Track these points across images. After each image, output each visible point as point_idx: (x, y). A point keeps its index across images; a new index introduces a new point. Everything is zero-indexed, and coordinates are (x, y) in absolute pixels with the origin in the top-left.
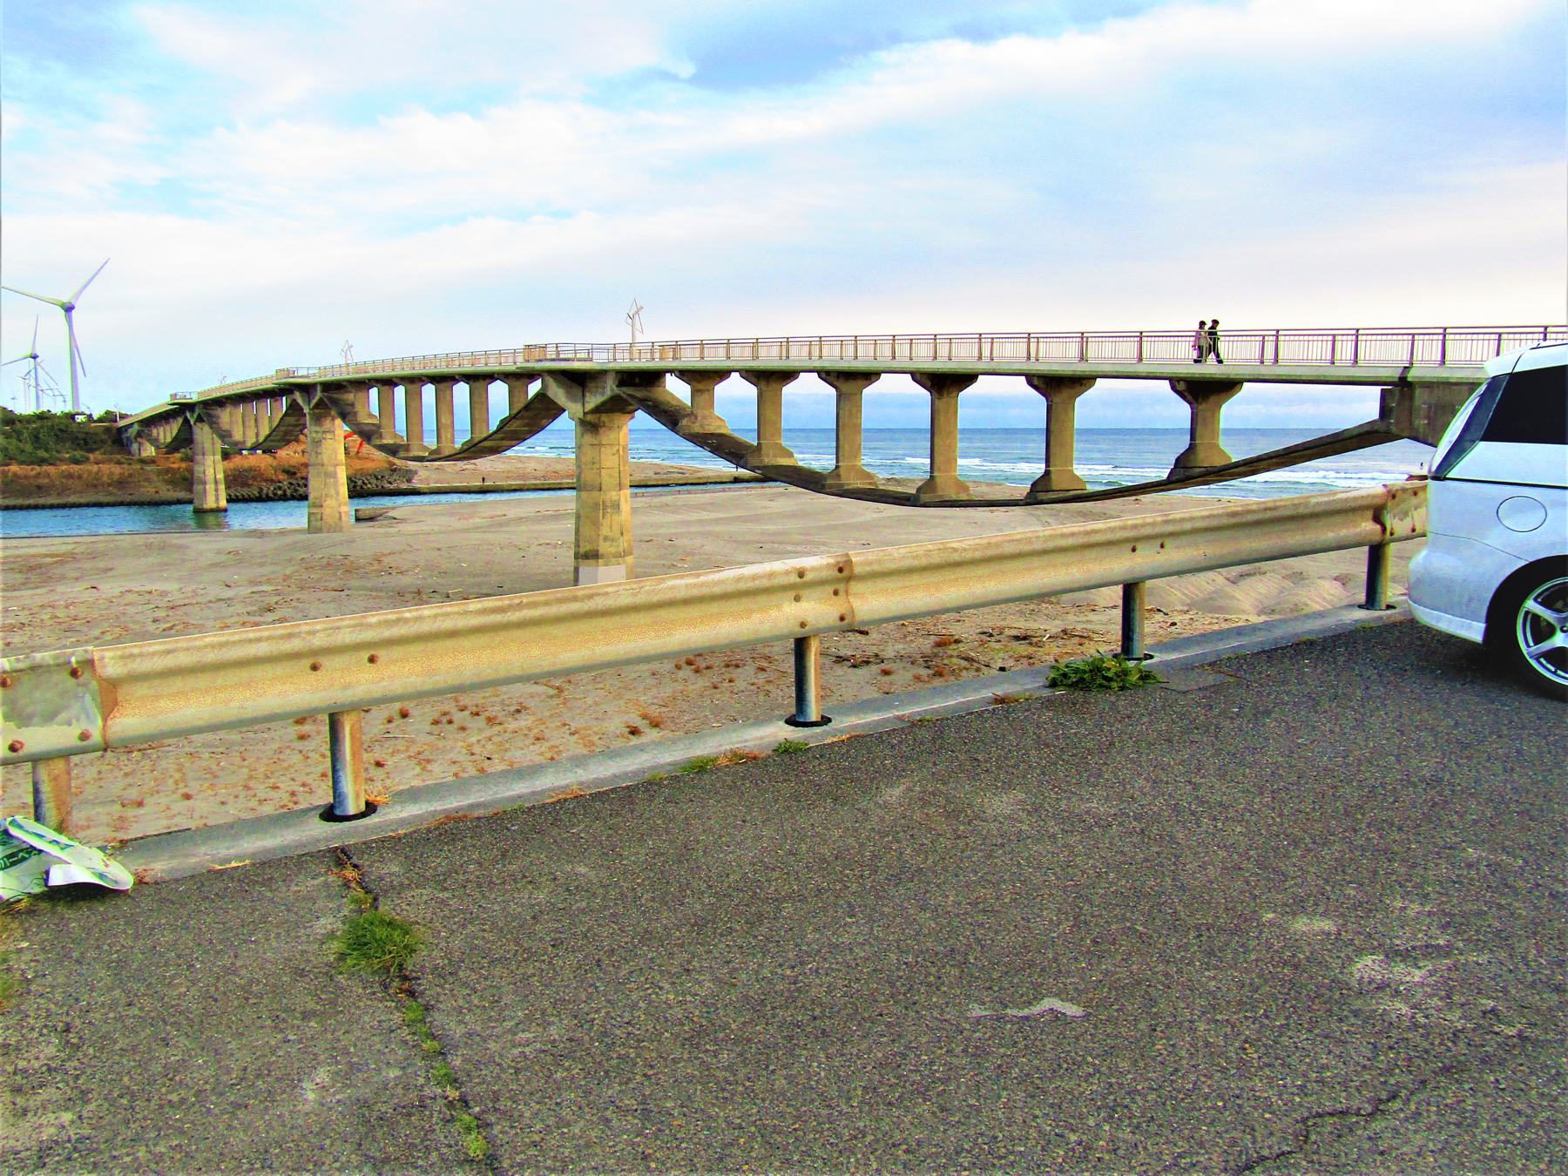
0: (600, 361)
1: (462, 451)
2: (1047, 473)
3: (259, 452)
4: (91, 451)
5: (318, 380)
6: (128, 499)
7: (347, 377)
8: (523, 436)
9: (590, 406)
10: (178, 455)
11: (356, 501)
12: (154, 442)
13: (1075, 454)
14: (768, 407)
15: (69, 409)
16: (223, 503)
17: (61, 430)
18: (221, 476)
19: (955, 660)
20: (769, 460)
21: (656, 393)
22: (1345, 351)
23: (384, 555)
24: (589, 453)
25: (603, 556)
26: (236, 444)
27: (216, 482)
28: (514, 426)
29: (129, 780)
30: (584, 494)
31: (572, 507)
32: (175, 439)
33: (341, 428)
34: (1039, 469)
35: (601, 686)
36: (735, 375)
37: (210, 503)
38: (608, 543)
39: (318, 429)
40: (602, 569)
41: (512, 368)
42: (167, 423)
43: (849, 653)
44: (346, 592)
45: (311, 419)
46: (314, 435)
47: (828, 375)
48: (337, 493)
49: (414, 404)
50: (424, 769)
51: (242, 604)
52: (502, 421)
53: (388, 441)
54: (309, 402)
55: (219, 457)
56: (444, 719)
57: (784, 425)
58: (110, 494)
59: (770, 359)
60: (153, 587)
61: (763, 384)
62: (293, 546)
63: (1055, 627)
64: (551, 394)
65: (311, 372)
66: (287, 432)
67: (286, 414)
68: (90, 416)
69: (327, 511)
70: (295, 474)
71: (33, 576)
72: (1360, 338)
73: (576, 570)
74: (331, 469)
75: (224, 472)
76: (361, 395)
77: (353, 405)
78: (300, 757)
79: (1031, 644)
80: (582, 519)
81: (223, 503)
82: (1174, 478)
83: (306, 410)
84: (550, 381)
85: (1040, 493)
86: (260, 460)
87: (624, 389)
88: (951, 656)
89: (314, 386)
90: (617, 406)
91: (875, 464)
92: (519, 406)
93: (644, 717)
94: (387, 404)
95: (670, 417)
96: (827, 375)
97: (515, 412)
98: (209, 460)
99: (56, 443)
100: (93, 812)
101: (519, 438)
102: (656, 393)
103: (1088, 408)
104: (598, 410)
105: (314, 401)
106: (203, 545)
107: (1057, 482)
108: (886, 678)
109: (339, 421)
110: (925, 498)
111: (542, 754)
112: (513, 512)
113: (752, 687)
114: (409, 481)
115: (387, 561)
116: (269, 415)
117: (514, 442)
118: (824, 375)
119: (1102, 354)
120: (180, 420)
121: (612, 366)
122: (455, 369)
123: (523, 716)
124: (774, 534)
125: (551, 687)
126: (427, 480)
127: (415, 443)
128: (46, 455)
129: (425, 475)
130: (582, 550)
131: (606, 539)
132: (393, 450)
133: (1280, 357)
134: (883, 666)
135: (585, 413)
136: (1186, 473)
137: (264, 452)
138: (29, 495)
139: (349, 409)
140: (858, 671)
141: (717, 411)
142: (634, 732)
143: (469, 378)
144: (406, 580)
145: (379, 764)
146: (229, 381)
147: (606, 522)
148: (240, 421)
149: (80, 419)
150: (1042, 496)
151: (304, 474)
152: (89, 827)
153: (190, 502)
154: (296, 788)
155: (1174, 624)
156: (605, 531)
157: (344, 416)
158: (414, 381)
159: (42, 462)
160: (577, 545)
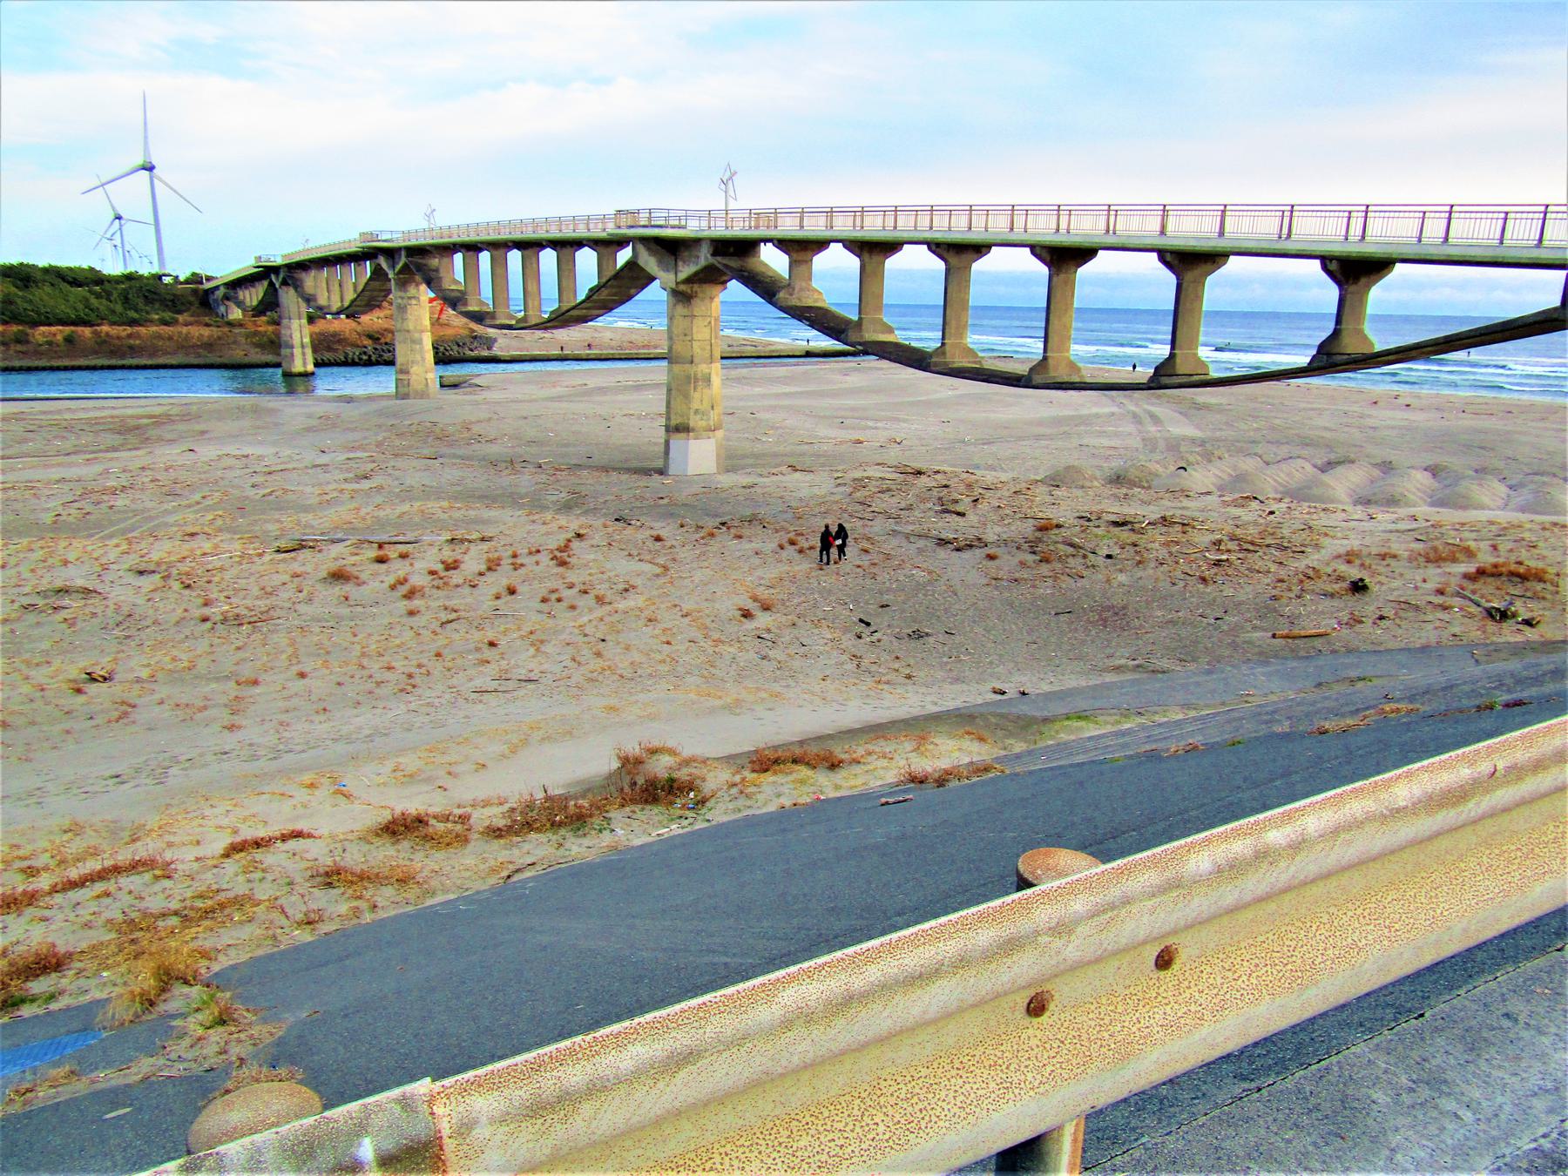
0: (693, 228)
1: (549, 321)
2: (1172, 356)
3: (343, 316)
4: (180, 312)
5: (402, 244)
6: (219, 361)
7: (431, 242)
8: (611, 305)
9: (683, 275)
10: (264, 319)
11: (441, 367)
12: (240, 304)
13: (1201, 339)
14: (869, 279)
15: (155, 270)
16: (310, 368)
17: (149, 291)
18: (307, 340)
19: (1061, 546)
20: (872, 335)
21: (751, 263)
22: (1434, 229)
23: (471, 423)
24: (681, 324)
25: (693, 430)
26: (320, 308)
27: (303, 346)
28: (604, 295)
29: (241, 655)
30: (677, 368)
31: (663, 378)
32: (261, 302)
33: (425, 293)
34: (1164, 351)
35: (706, 564)
36: (836, 248)
37: (298, 367)
38: (698, 417)
39: (402, 294)
40: (692, 442)
41: (604, 235)
42: (253, 286)
43: (951, 536)
44: (441, 460)
45: (397, 284)
46: (400, 301)
47: (938, 248)
48: (423, 359)
49: (500, 271)
50: (538, 650)
51: (337, 472)
52: (591, 290)
53: (473, 308)
54: (394, 267)
55: (304, 321)
56: (554, 596)
57: (885, 301)
58: (199, 356)
59: (874, 228)
60: (248, 450)
61: (866, 256)
62: (381, 413)
63: (1153, 513)
64: (641, 262)
65: (395, 236)
66: (370, 299)
67: (371, 279)
68: (177, 277)
69: (414, 378)
70: (378, 339)
71: (132, 440)
72: (1548, 216)
73: (667, 443)
74: (417, 335)
75: (311, 336)
76: (446, 260)
77: (437, 270)
78: (411, 633)
79: (1133, 530)
80: (673, 392)
81: (310, 368)
82: (1315, 365)
83: (391, 276)
84: (641, 249)
85: (1164, 377)
86: (343, 325)
87: (719, 258)
88: (1057, 542)
89: (399, 249)
90: (711, 277)
91: (981, 342)
92: (609, 273)
93: (755, 599)
94: (471, 269)
95: (766, 288)
96: (937, 247)
97: (604, 280)
98: (295, 324)
99: (146, 305)
100: (207, 689)
101: (608, 307)
102: (751, 263)
103: (1218, 288)
104: (689, 281)
105: (398, 267)
106: (293, 410)
107: (1182, 367)
108: (991, 563)
109: (423, 287)
110: (1037, 379)
111: (656, 637)
112: (593, 382)
113: (858, 570)
114: (489, 348)
115: (476, 429)
116: (355, 278)
117: (601, 312)
118: (934, 248)
119: (1241, 229)
120: (266, 283)
121: (706, 234)
122: (542, 234)
123: (632, 593)
124: (853, 409)
125: (657, 564)
126: (509, 348)
127: (501, 310)
128: (135, 315)
129: (505, 343)
130: (673, 422)
131: (697, 412)
132: (478, 317)
133: (1294, 231)
134: (987, 551)
135: (677, 283)
136: (1329, 359)
137: (348, 317)
138: (123, 356)
139: (433, 275)
140: (966, 555)
141: (815, 284)
142: (747, 615)
143: (557, 244)
144: (493, 450)
145: (492, 644)
146: (310, 245)
147: (696, 395)
148: (324, 285)
149: (167, 280)
150: (1165, 380)
151: (388, 340)
152: (205, 708)
153: (278, 365)
154: (412, 670)
155: (1272, 513)
156: (695, 405)
157: (429, 283)
158: (499, 247)
159: (133, 323)
160: (668, 419)
